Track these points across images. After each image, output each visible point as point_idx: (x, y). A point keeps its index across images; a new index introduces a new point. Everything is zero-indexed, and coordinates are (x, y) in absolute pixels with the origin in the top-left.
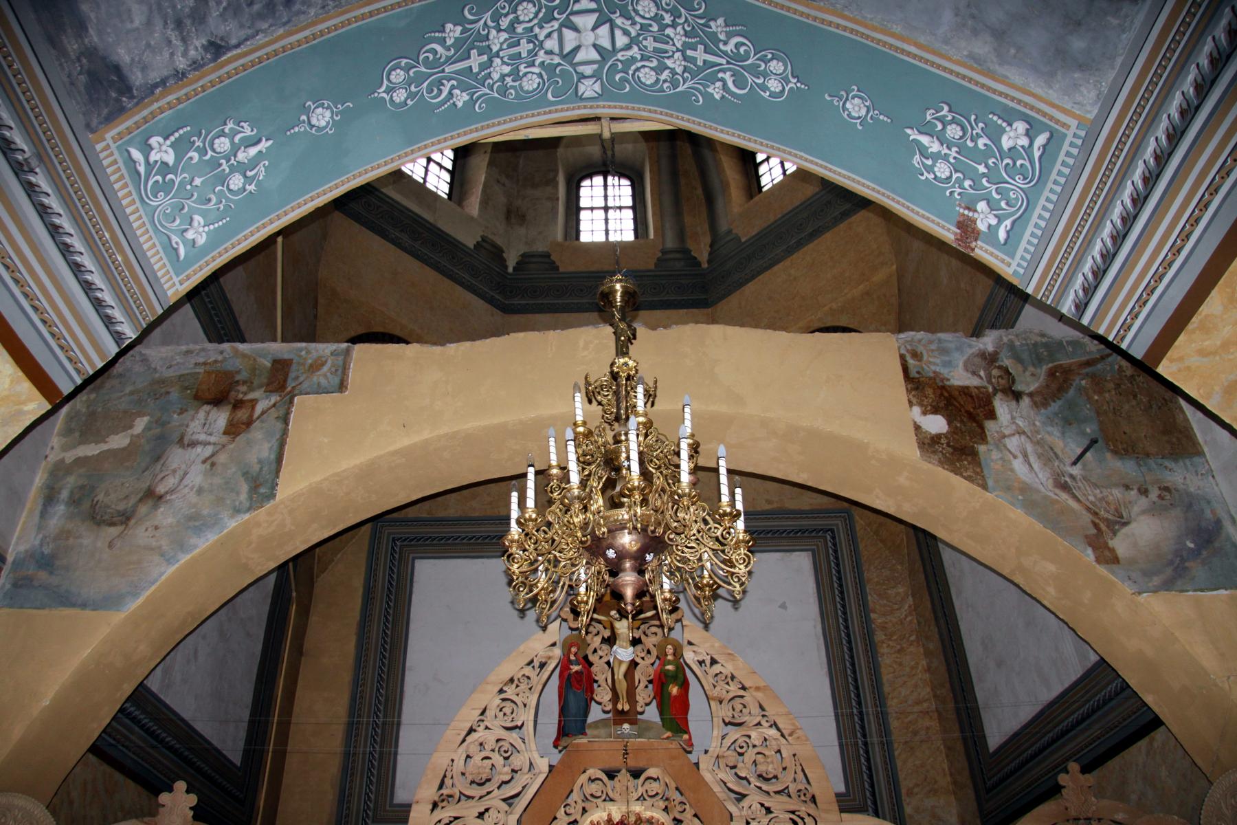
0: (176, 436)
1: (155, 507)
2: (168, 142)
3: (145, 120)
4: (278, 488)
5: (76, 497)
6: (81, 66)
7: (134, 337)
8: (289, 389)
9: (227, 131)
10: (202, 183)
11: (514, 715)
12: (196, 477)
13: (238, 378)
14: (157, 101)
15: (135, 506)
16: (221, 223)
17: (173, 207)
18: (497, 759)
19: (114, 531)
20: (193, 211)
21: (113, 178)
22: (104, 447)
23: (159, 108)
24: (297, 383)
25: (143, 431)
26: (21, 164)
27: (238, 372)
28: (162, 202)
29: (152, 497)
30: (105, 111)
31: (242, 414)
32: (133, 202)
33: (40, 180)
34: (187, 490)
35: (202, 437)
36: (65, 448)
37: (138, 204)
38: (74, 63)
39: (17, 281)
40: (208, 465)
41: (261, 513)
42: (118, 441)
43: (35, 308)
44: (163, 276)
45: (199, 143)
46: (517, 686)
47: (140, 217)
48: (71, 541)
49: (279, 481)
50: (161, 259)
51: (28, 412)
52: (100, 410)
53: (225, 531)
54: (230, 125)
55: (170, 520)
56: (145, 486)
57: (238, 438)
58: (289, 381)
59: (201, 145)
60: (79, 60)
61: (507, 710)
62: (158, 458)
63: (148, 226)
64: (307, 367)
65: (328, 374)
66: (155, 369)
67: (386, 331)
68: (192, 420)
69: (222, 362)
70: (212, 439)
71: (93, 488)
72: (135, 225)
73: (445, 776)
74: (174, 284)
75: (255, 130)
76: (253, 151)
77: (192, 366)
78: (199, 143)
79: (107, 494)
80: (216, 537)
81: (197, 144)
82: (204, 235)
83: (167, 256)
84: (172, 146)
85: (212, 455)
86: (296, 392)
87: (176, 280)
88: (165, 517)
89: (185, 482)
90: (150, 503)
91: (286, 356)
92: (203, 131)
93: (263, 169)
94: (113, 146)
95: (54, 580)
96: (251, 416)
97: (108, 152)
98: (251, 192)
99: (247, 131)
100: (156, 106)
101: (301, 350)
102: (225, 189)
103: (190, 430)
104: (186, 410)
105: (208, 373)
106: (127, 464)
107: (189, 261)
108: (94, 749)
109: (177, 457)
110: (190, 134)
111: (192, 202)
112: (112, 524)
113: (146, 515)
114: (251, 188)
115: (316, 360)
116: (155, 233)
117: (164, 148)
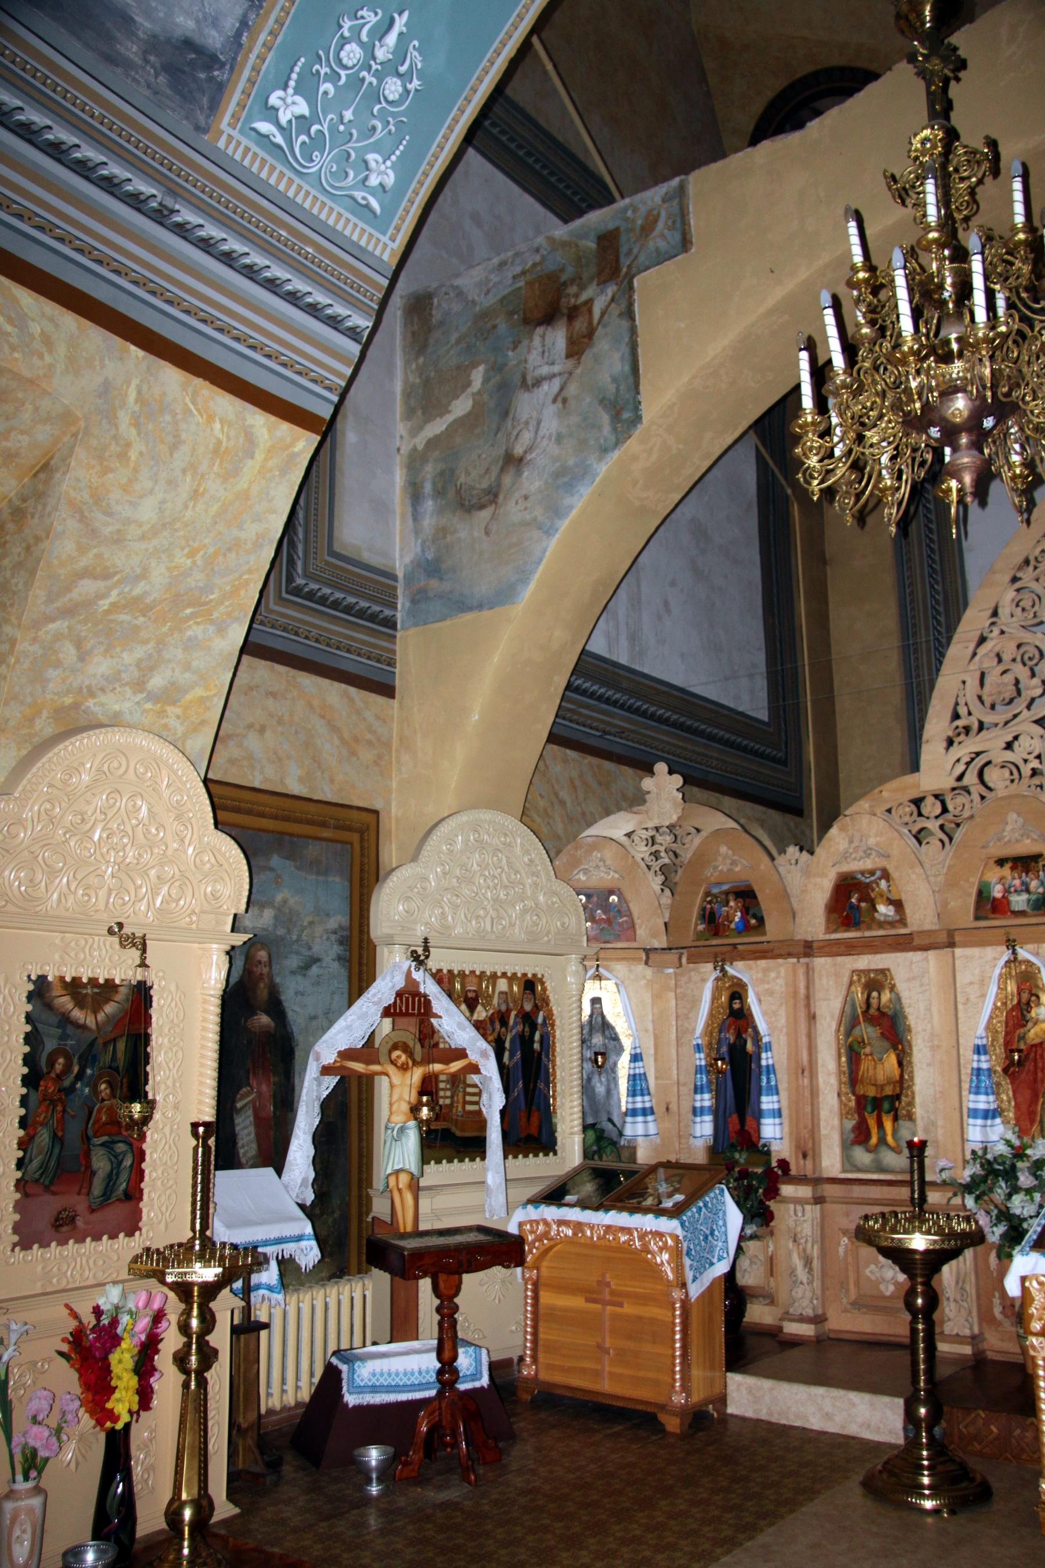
0: (517, 379)
1: (519, 473)
2: (290, 91)
3: (252, 82)
4: (643, 407)
5: (440, 486)
6: (153, 67)
7: (370, 324)
8: (624, 270)
9: (347, 34)
10: (354, 113)
11: (1036, 608)
12: (551, 424)
13: (564, 277)
14: (250, 51)
15: (499, 478)
16: (401, 148)
17: (336, 160)
18: (1021, 671)
19: (485, 514)
20: (362, 152)
21: (254, 169)
22: (450, 418)
23: (258, 57)
24: (632, 258)
25: (483, 384)
26: (159, 211)
27: (562, 270)
28: (322, 162)
29: (513, 462)
30: (205, 101)
31: (580, 325)
32: (291, 181)
33: (187, 215)
34: (545, 442)
35: (545, 370)
36: (414, 432)
37: (297, 180)
38: (143, 68)
39: (221, 330)
40: (559, 404)
41: (633, 445)
42: (461, 406)
43: (253, 347)
44: (368, 243)
45: (324, 70)
46: (1036, 568)
47: (308, 194)
48: (449, 538)
49: (642, 398)
50: (356, 225)
51: (301, 452)
52: (432, 374)
53: (598, 480)
54: (347, 24)
55: (537, 484)
56: (502, 451)
57: (584, 357)
58: (622, 259)
59: (328, 70)
60: (147, 62)
61: (1026, 603)
62: (505, 414)
63: (322, 198)
64: (638, 232)
65: (666, 232)
66: (473, 301)
67: (819, 67)
68: (529, 352)
69: (540, 263)
70: (556, 369)
71: (452, 471)
72: (307, 205)
73: (957, 704)
74: (385, 245)
75: (380, 11)
76: (391, 39)
77: (510, 281)
78: (324, 70)
79: (468, 474)
80: (590, 490)
81: (322, 73)
82: (390, 172)
83: (360, 219)
84: (297, 92)
85: (562, 389)
86: (634, 271)
87: (385, 239)
88: (532, 481)
89: (541, 433)
90: (512, 470)
91: (611, 226)
92: (321, 52)
93: (415, 53)
94: (235, 134)
95: (446, 586)
96: (590, 323)
97: (234, 142)
98: (416, 90)
99: (371, 18)
100: (252, 57)
101: (625, 210)
102: (384, 104)
103: (530, 366)
104: (520, 342)
105: (529, 284)
106: (477, 431)
107: (389, 211)
108: (553, 738)
109: (526, 405)
110: (308, 67)
111: (357, 141)
112: (482, 507)
113: (514, 484)
114: (415, 84)
115: (647, 218)
116: (333, 201)
117: (289, 100)
